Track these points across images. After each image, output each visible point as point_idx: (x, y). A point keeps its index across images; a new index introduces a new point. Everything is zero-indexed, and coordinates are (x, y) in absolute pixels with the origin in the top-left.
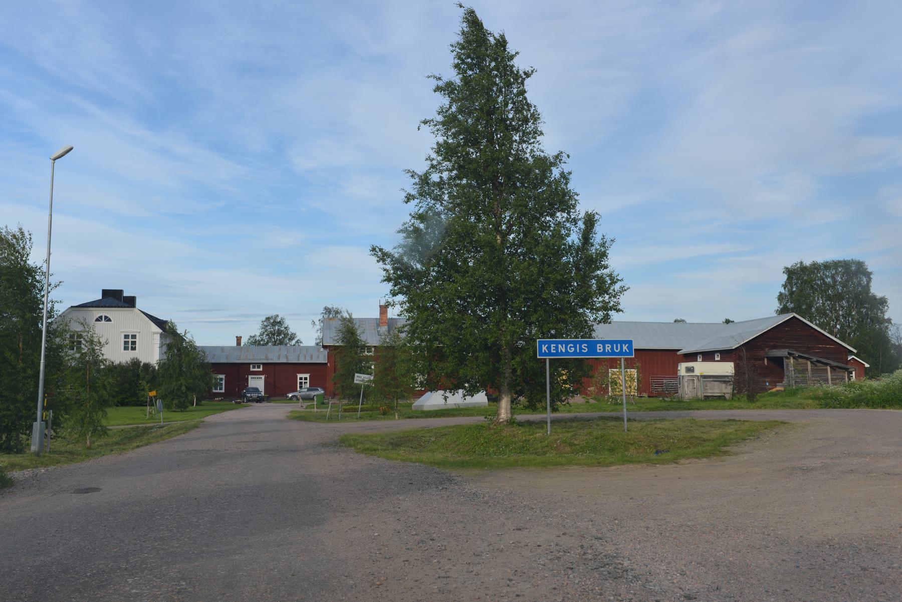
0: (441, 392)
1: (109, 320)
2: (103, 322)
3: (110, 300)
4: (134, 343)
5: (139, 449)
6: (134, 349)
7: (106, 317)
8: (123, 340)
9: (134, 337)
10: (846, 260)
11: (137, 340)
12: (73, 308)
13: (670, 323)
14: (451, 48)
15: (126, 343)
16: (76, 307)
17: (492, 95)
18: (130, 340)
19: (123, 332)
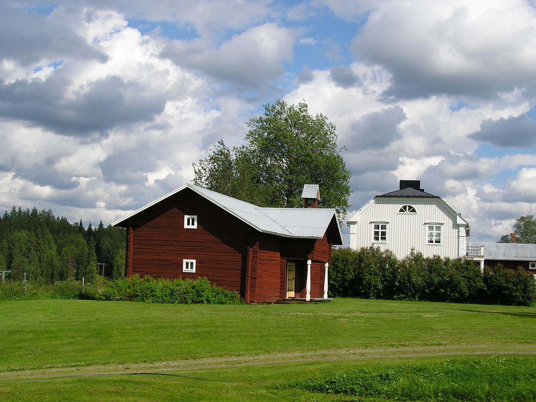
0: (328, 266)
1: (414, 211)
2: (407, 212)
3: (410, 191)
4: (383, 234)
5: (222, 305)
6: (384, 238)
7: (410, 207)
8: (373, 230)
9: (384, 227)
10: (39, 211)
11: (387, 231)
12: (378, 198)
13: (456, 222)
14: (220, 141)
15: (376, 233)
16: (381, 196)
17: (309, 124)
18: (380, 230)
19: (374, 222)
